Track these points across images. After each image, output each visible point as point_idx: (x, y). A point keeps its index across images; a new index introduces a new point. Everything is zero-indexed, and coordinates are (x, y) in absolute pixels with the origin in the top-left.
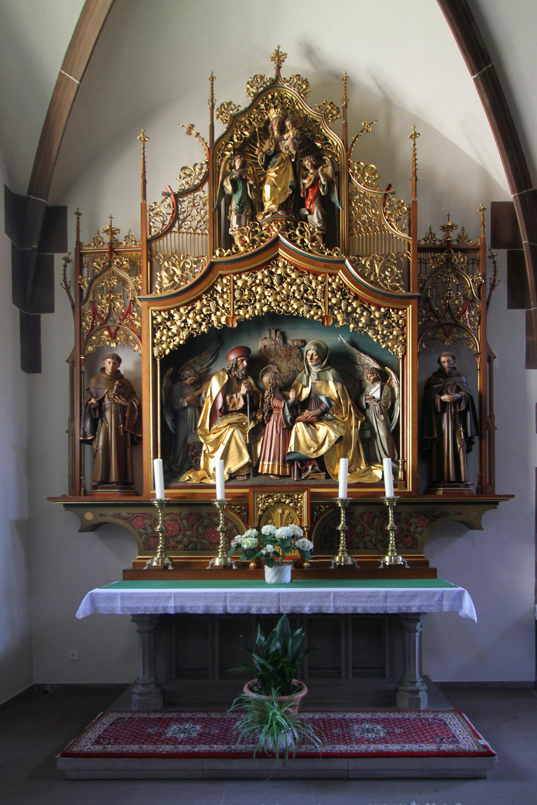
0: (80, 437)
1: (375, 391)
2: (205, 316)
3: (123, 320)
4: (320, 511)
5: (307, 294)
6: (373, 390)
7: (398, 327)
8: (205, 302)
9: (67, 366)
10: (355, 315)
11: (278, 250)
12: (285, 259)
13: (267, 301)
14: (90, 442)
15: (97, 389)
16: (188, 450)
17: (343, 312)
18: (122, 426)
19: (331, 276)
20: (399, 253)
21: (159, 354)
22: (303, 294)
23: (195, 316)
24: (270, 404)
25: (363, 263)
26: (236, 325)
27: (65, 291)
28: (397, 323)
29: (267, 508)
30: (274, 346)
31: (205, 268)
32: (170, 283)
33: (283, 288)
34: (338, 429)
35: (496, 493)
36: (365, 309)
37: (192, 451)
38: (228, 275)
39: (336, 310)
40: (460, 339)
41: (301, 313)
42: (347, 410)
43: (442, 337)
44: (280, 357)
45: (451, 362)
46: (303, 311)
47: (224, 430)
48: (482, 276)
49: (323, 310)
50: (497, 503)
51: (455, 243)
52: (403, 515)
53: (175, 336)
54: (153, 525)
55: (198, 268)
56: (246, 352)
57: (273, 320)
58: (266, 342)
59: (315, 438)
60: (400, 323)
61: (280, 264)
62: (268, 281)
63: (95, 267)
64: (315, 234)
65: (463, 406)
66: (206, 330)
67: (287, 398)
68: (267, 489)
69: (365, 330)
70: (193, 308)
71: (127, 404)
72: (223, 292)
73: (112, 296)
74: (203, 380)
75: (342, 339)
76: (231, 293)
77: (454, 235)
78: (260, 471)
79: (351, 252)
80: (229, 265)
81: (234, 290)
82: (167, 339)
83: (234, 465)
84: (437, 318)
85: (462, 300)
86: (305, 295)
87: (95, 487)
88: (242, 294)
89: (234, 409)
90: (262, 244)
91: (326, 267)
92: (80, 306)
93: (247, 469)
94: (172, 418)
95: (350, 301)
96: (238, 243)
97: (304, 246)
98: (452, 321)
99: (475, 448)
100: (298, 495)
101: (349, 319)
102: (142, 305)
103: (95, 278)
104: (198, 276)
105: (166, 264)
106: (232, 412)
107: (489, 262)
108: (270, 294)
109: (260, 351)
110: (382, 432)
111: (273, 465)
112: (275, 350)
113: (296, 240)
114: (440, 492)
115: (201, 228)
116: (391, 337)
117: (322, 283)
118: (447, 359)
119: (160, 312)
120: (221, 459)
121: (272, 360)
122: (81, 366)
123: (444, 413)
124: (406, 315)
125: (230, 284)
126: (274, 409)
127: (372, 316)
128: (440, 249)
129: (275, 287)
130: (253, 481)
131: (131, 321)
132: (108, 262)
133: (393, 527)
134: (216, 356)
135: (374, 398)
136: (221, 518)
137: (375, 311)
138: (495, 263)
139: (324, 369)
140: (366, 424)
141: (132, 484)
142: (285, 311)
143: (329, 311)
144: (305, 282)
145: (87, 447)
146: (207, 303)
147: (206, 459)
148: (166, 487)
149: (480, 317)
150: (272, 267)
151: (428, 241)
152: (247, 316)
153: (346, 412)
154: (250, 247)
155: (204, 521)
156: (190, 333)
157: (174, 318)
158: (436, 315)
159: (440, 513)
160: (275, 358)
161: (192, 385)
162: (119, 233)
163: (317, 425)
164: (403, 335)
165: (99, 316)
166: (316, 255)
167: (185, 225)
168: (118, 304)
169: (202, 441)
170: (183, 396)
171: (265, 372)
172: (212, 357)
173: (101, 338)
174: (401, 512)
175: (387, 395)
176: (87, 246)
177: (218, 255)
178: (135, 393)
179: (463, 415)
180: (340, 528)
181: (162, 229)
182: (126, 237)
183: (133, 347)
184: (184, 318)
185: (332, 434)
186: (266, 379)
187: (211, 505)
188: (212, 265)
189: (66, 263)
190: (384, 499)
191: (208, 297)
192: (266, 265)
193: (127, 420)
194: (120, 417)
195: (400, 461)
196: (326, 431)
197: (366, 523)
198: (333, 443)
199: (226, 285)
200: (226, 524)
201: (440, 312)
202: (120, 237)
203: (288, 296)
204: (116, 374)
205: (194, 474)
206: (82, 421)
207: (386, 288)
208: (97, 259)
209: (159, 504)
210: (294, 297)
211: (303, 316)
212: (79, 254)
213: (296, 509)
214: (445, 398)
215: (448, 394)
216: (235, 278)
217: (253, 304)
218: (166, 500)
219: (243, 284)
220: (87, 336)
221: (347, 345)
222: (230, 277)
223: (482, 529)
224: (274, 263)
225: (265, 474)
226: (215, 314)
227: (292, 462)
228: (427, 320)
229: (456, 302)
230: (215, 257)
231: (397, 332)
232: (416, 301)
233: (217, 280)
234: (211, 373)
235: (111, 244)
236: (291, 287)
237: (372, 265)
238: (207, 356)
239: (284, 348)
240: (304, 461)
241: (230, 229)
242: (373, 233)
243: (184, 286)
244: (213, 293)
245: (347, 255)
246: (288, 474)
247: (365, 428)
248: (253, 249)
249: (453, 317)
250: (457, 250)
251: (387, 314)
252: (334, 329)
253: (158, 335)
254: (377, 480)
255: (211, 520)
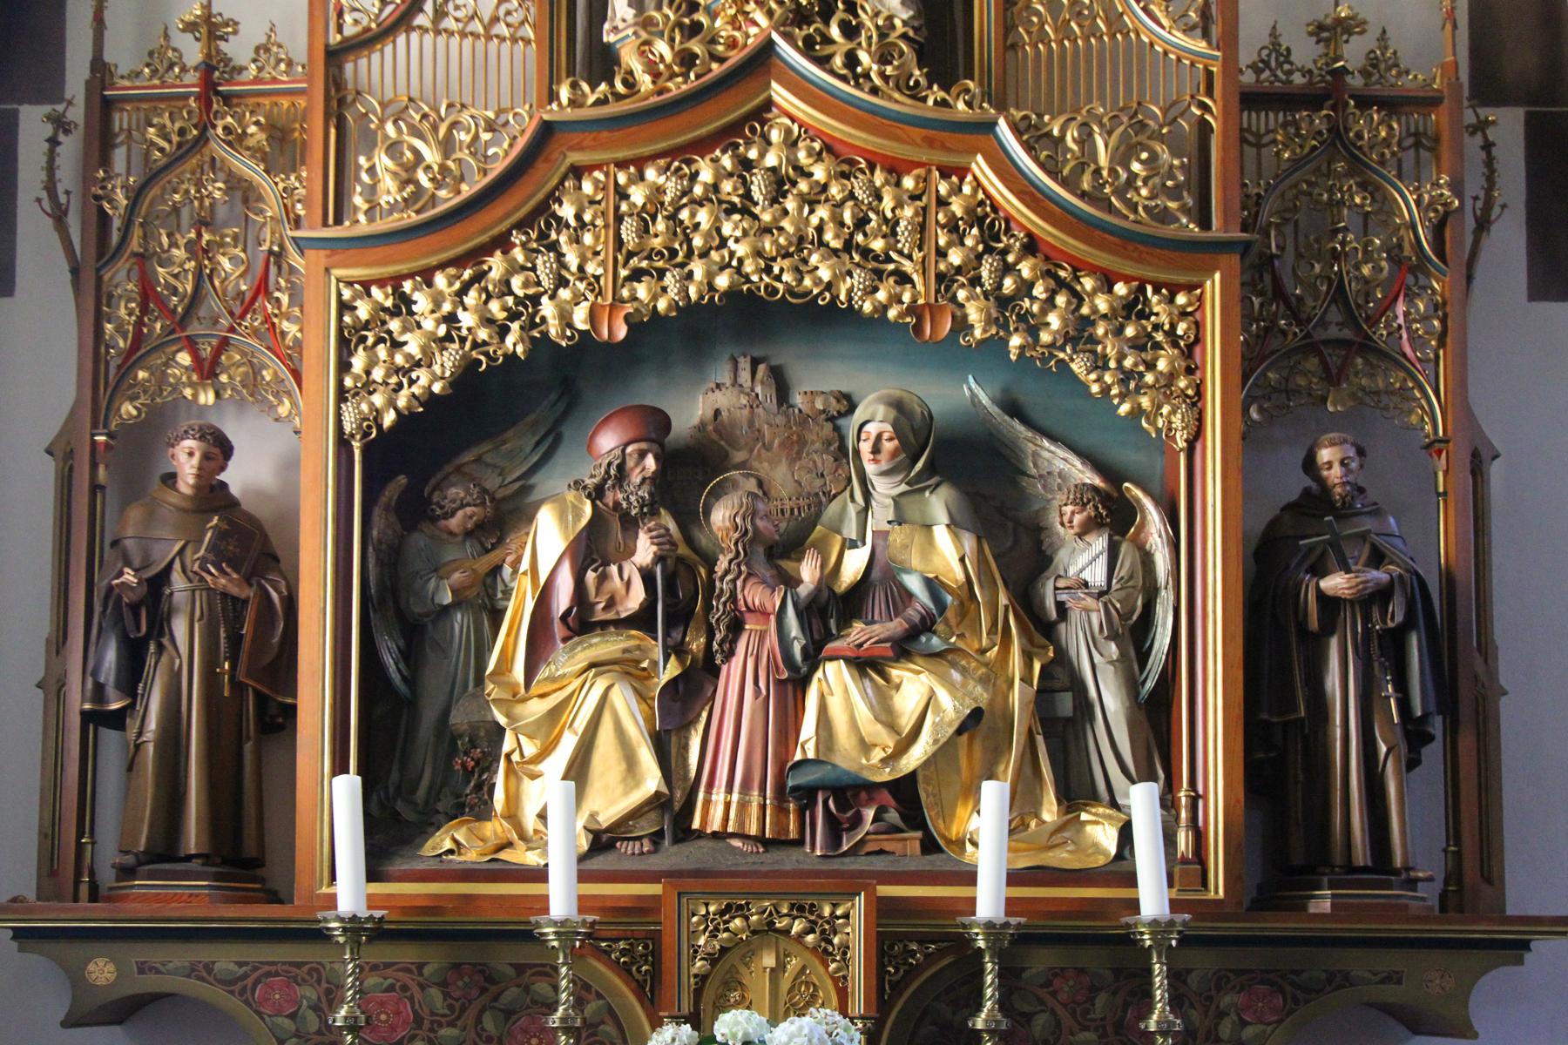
0: (83, 701)
1: (1085, 561)
2: (519, 301)
3: (242, 317)
4: (906, 963)
5: (865, 235)
6: (1083, 559)
7: (1175, 345)
8: (518, 254)
9: (49, 467)
10: (1026, 303)
11: (768, 86)
12: (793, 120)
13: (730, 256)
14: (117, 721)
15: (144, 540)
16: (453, 751)
17: (986, 295)
18: (227, 666)
19: (945, 175)
20: (1174, 103)
21: (360, 427)
22: (852, 235)
23: (486, 302)
24: (733, 597)
25: (1056, 132)
26: (622, 332)
27: (50, 221)
28: (1171, 333)
29: (724, 950)
30: (746, 412)
31: (521, 143)
32: (401, 189)
33: (786, 212)
34: (964, 685)
35: (1510, 911)
36: (1061, 284)
37: (466, 753)
38: (599, 167)
39: (963, 285)
40: (1377, 393)
41: (843, 297)
42: (994, 624)
43: (1317, 387)
44: (768, 447)
45: (1354, 465)
46: (850, 291)
47: (577, 683)
48: (1450, 186)
49: (920, 287)
50: (1525, 945)
51: (1356, 82)
52: (1193, 980)
53: (419, 358)
54: (324, 1005)
55: (499, 145)
56: (654, 426)
57: (748, 321)
58: (723, 400)
59: (886, 714)
60: (1180, 332)
61: (775, 136)
62: (735, 189)
63: (152, 143)
64: (893, 37)
65: (1397, 612)
66: (520, 349)
67: (792, 582)
68: (730, 887)
69: (1062, 355)
70: (479, 277)
71: (249, 593)
72: (582, 225)
73: (206, 237)
74: (505, 518)
75: (975, 392)
76: (606, 226)
77: (1353, 53)
78: (696, 825)
79: (1011, 96)
80: (605, 134)
81: (619, 219)
82: (388, 375)
83: (611, 800)
84: (1299, 323)
85: (1384, 264)
86: (860, 238)
87: (126, 872)
88: (647, 231)
89: (610, 616)
90: (714, 66)
91: (930, 143)
92: (98, 270)
93: (653, 815)
94: (401, 643)
95: (1011, 258)
96: (631, 59)
97: (856, 77)
98: (1347, 334)
99: (1433, 754)
100: (835, 906)
101: (1006, 320)
102: (306, 268)
103: (152, 178)
104: (497, 168)
105: (390, 128)
106: (604, 625)
107: (1473, 143)
108: (738, 233)
109: (702, 426)
110: (1111, 699)
111: (743, 806)
112: (751, 423)
113: (829, 57)
114: (1322, 903)
115: (510, 19)
116: (1149, 378)
117: (915, 197)
118: (1339, 456)
119: (366, 285)
120: (565, 778)
121: (739, 456)
122: (94, 466)
123: (1332, 633)
124: (1201, 307)
125: (606, 197)
126: (747, 616)
127: (1085, 310)
128: (1310, 100)
129: (757, 210)
130: (673, 856)
131: (267, 319)
132: (195, 126)
133: (1169, 1022)
134: (550, 445)
135: (1086, 584)
136: (564, 983)
137: (1095, 291)
138: (1488, 146)
139: (917, 487)
140: (1058, 672)
141: (256, 863)
142: (789, 290)
143: (938, 291)
144: (859, 193)
145: (109, 736)
146: (527, 259)
147: (513, 780)
148: (373, 875)
149: (1444, 321)
150: (749, 143)
151: (1267, 73)
152: (662, 305)
153: (992, 630)
154: (672, 76)
155: (500, 994)
156: (464, 357)
157: (415, 308)
158: (1295, 312)
159: (1323, 976)
160: (751, 451)
161: (468, 534)
162: (235, 32)
163: (895, 673)
164: (1190, 371)
165: (162, 303)
166: (900, 104)
167: (457, 8)
168: (226, 263)
169: (502, 720)
170: (438, 569)
171: (717, 494)
172: (538, 444)
173: (164, 373)
174: (1189, 971)
175: (1131, 577)
176: (129, 77)
177: (565, 101)
178: (276, 559)
179: (1394, 643)
180: (980, 1023)
181: (378, 16)
182: (257, 49)
183: (272, 407)
184: (447, 307)
185: (945, 699)
186: (721, 516)
187: (528, 936)
188: (547, 131)
189: (56, 133)
190: (1136, 925)
191: (529, 240)
192: (727, 136)
193: (246, 644)
194: (223, 635)
195: (1182, 794)
196: (925, 691)
197: (1064, 1005)
198: (951, 731)
199: (592, 202)
200: (579, 1003)
201: (1310, 303)
202: (238, 49)
203: (801, 239)
204: (213, 496)
205: (470, 830)
206: (92, 649)
207: (1132, 217)
208: (160, 115)
209: (345, 930)
210: (822, 244)
211: (851, 306)
212: (97, 99)
213: (825, 955)
214: (1335, 583)
215: (1348, 571)
216: (622, 178)
217: (682, 265)
218: (371, 918)
219: (649, 199)
220: (119, 367)
221: (994, 410)
222: (607, 175)
223: (1475, 1036)
224: (753, 130)
225: (715, 835)
226: (552, 297)
227: (807, 796)
228: (1267, 329)
229: (1366, 270)
230: (554, 106)
231: (1171, 363)
232: (1235, 259)
233: (562, 182)
234: (535, 496)
235: (207, 68)
236: (812, 212)
237: (1086, 140)
238: (521, 441)
239: (780, 420)
240: (849, 792)
241: (607, 26)
242: (1087, 40)
243: (447, 199)
244: (549, 226)
245: (1002, 107)
246: (793, 835)
247: (1057, 685)
248: (685, 82)
249: (1351, 319)
250: (1364, 102)
251: (1136, 301)
252: (955, 353)
253: (358, 362)
254: (1101, 861)
255: (527, 989)
